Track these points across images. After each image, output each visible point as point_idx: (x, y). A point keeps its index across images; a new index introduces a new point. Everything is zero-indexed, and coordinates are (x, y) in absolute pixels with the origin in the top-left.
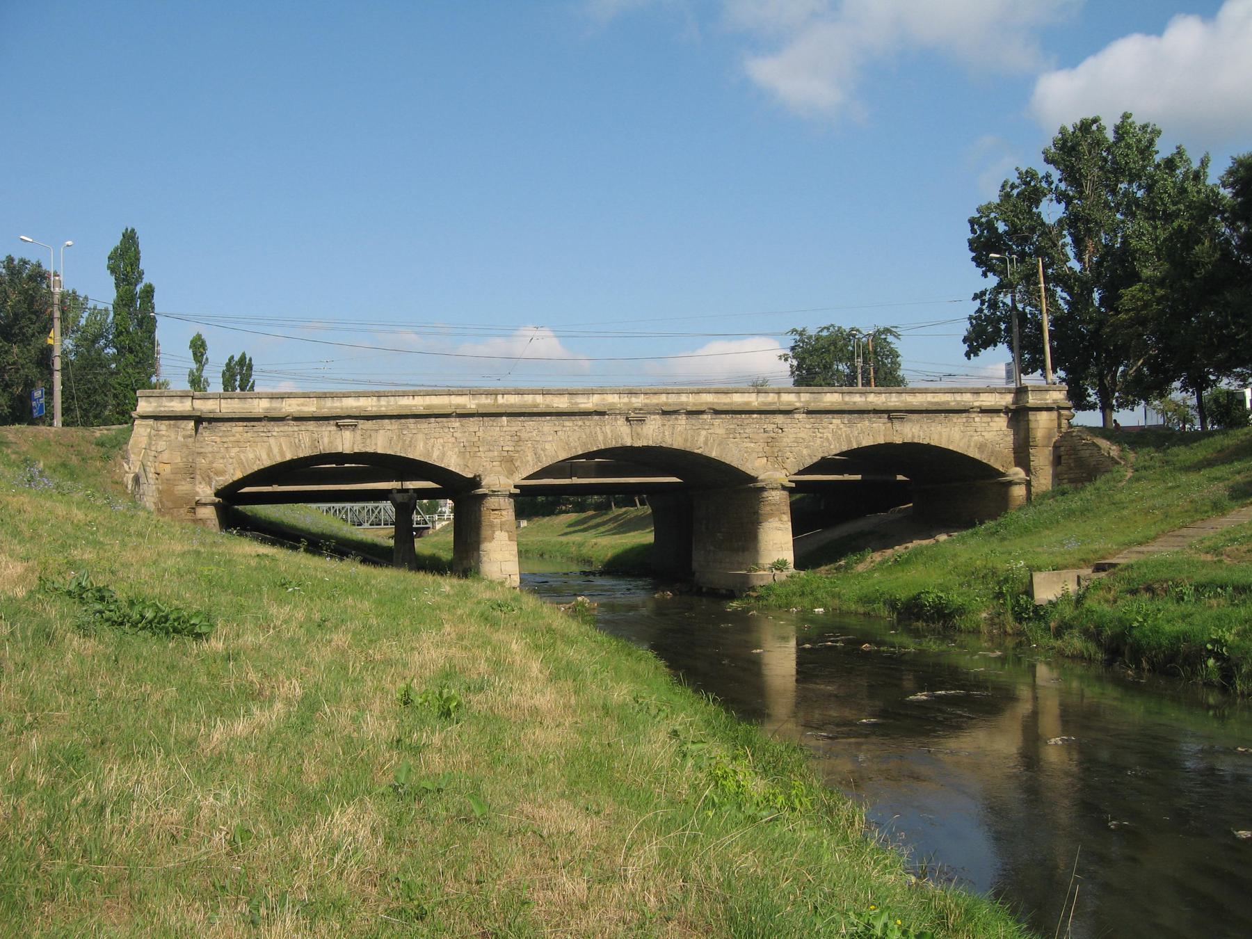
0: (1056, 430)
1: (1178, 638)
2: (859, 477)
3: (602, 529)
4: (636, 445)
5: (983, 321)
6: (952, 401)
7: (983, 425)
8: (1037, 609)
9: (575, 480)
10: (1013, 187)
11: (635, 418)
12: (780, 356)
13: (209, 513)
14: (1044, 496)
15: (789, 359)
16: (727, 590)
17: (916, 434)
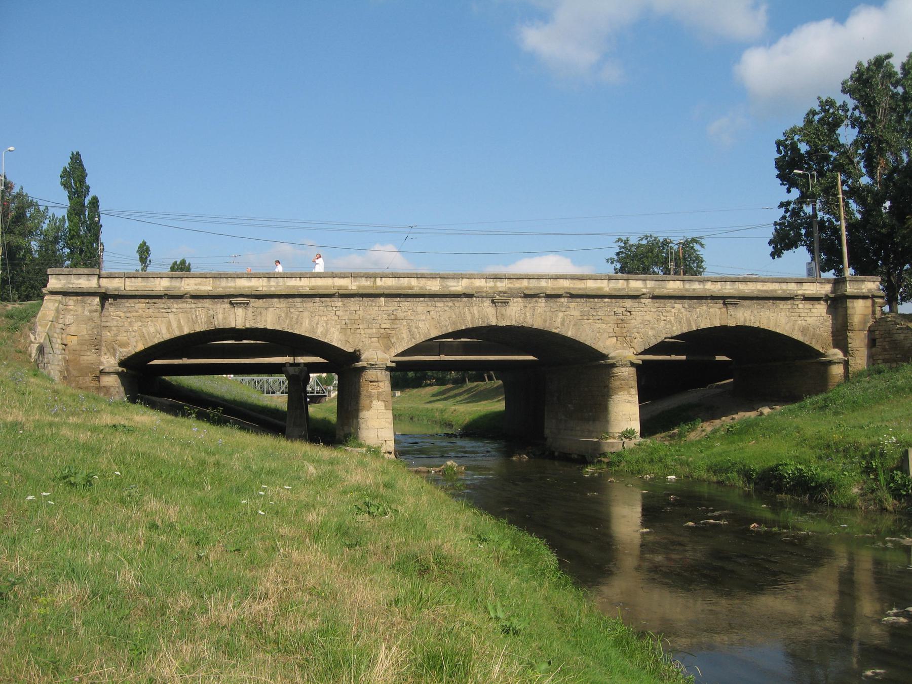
0: (870, 316)
2: (684, 357)
3: (458, 399)
4: (500, 324)
5: (785, 227)
6: (779, 290)
7: (806, 311)
9: (443, 358)
10: (814, 113)
11: (499, 300)
12: (607, 260)
13: (112, 381)
14: (860, 374)
15: (615, 262)
16: (578, 455)
17: (748, 319)
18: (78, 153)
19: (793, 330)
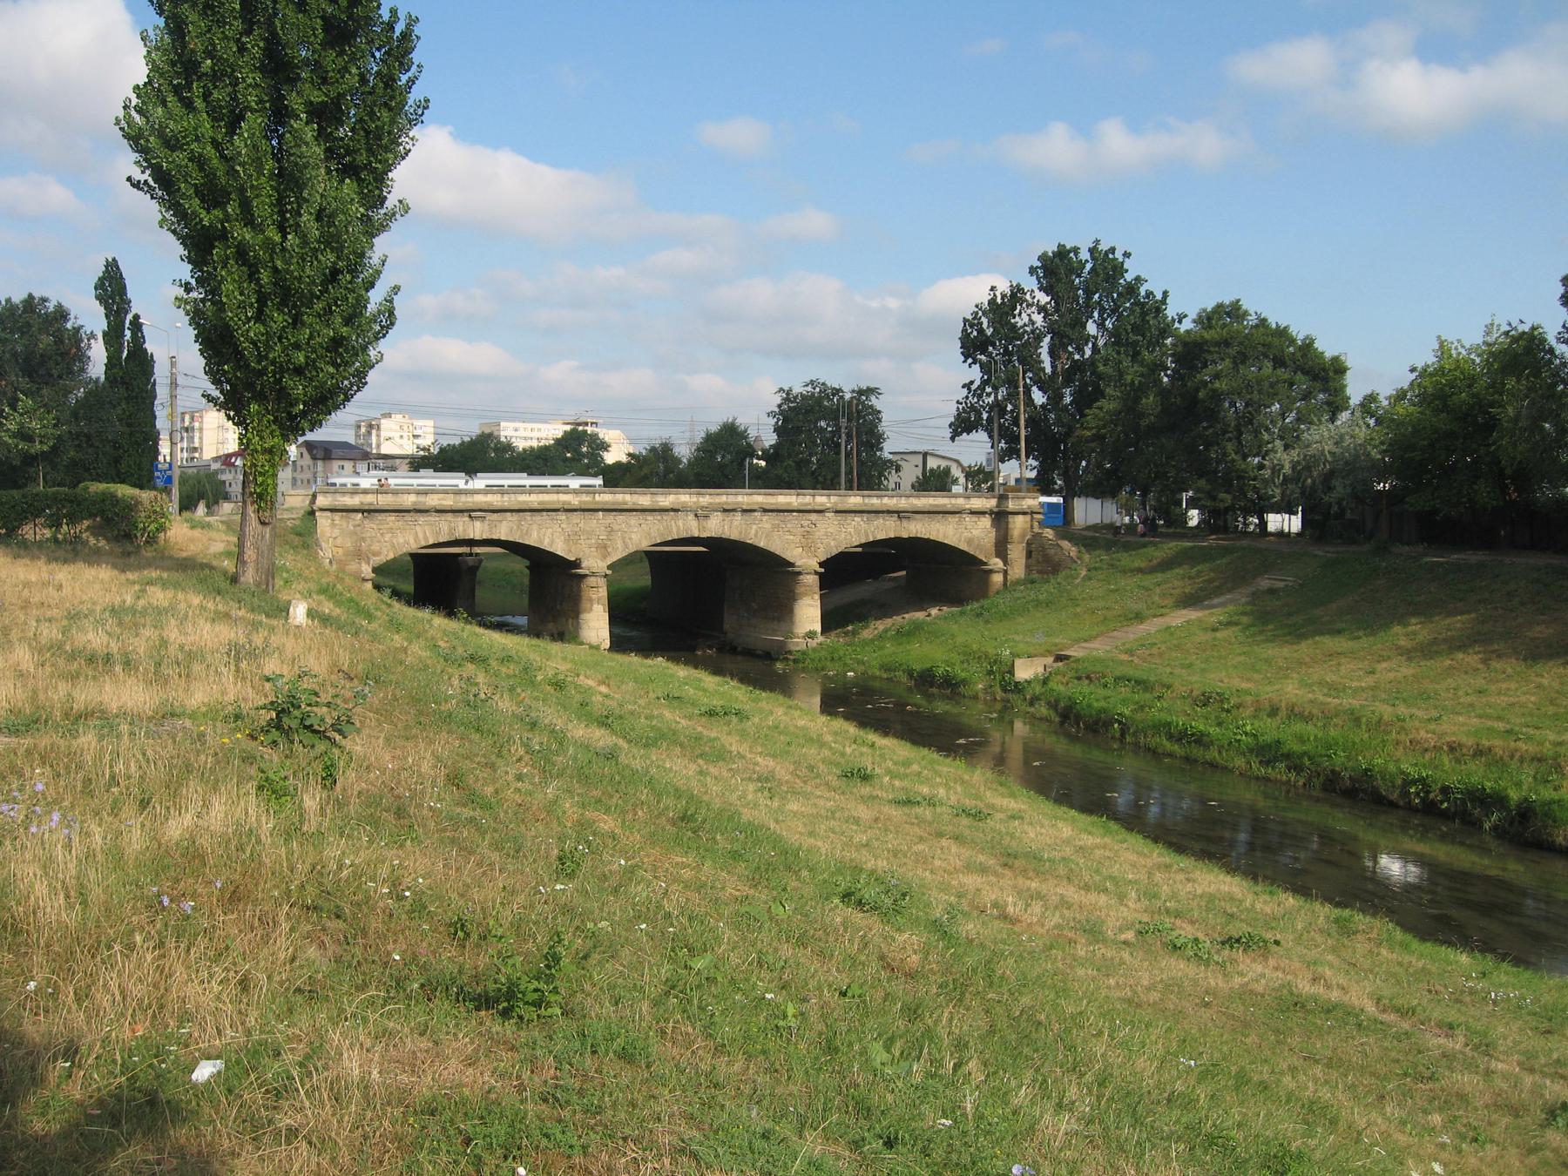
1: (1100, 711)
8: (1017, 683)
14: (1018, 582)
18: (114, 259)
19: (960, 541)
